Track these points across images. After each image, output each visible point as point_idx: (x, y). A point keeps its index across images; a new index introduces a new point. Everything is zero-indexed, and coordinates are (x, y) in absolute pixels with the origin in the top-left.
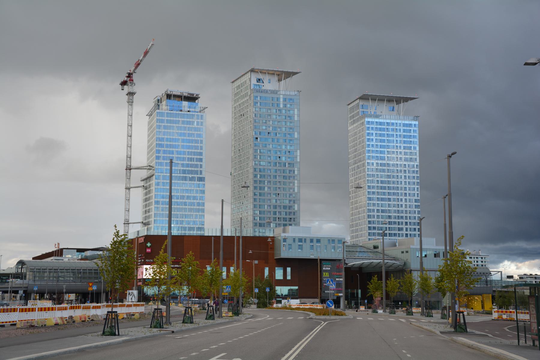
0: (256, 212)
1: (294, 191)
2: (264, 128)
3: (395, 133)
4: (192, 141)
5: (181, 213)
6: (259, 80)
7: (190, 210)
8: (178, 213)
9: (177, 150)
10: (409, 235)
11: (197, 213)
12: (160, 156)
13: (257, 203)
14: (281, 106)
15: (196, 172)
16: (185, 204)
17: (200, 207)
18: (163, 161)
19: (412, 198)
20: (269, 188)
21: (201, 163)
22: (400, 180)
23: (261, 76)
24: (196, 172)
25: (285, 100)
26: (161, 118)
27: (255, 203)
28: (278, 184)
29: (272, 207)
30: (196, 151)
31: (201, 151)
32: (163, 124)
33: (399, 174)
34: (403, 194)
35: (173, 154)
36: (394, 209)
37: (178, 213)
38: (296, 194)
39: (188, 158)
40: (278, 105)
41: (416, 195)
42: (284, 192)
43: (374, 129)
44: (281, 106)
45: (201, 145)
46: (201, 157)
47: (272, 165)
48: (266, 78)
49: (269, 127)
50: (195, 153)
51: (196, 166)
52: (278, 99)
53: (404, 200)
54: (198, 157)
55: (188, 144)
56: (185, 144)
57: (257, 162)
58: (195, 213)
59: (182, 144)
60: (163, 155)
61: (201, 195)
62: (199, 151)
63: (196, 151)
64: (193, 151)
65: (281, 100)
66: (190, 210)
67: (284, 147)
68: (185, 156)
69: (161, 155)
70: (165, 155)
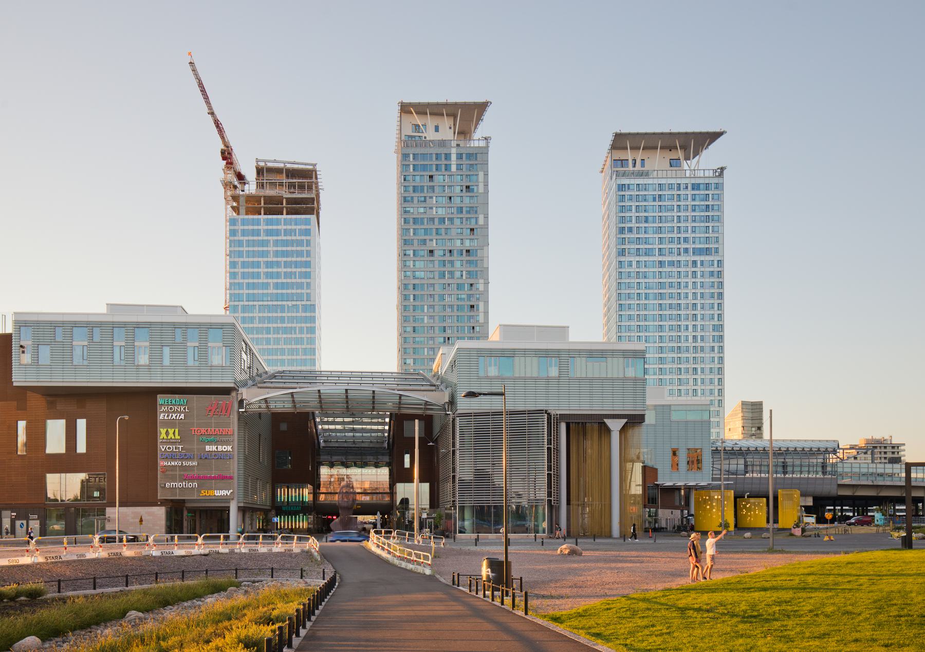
0: (408, 252)
1: (477, 223)
2: (422, 210)
3: (675, 203)
4: (292, 243)
5: (275, 325)
6: (417, 127)
7: (291, 320)
8: (270, 325)
9: (266, 259)
10: (699, 263)
11: (303, 325)
12: (237, 231)
13: (410, 313)
14: (454, 168)
15: (299, 297)
16: (282, 352)
17: (308, 357)
18: (241, 238)
19: (707, 323)
20: (431, 317)
21: (308, 238)
22: (683, 291)
23: (418, 120)
24: (299, 297)
25: (460, 156)
26: (237, 249)
27: (407, 303)
28: (449, 310)
29: (436, 297)
30: (299, 259)
31: (308, 259)
32: (242, 259)
33: (683, 280)
34: (691, 371)
35: (259, 267)
36: (671, 345)
37: (270, 325)
38: (481, 326)
39: (285, 230)
40: (448, 167)
41: (716, 316)
42: (459, 324)
43: (634, 198)
44: (454, 168)
45: (308, 248)
46: (308, 227)
47: (437, 277)
48: (430, 122)
49: (431, 208)
50: (296, 265)
51: (300, 286)
52: (448, 156)
53: (690, 328)
54: (303, 227)
55: (284, 249)
56: (280, 249)
57: (408, 274)
58: (299, 325)
59: (275, 249)
60: (242, 270)
61: (309, 336)
62: (304, 259)
63: (299, 259)
64: (294, 259)
65: (454, 157)
66: (291, 320)
67: (458, 243)
68: (279, 270)
69: (240, 227)
70: (246, 227)
